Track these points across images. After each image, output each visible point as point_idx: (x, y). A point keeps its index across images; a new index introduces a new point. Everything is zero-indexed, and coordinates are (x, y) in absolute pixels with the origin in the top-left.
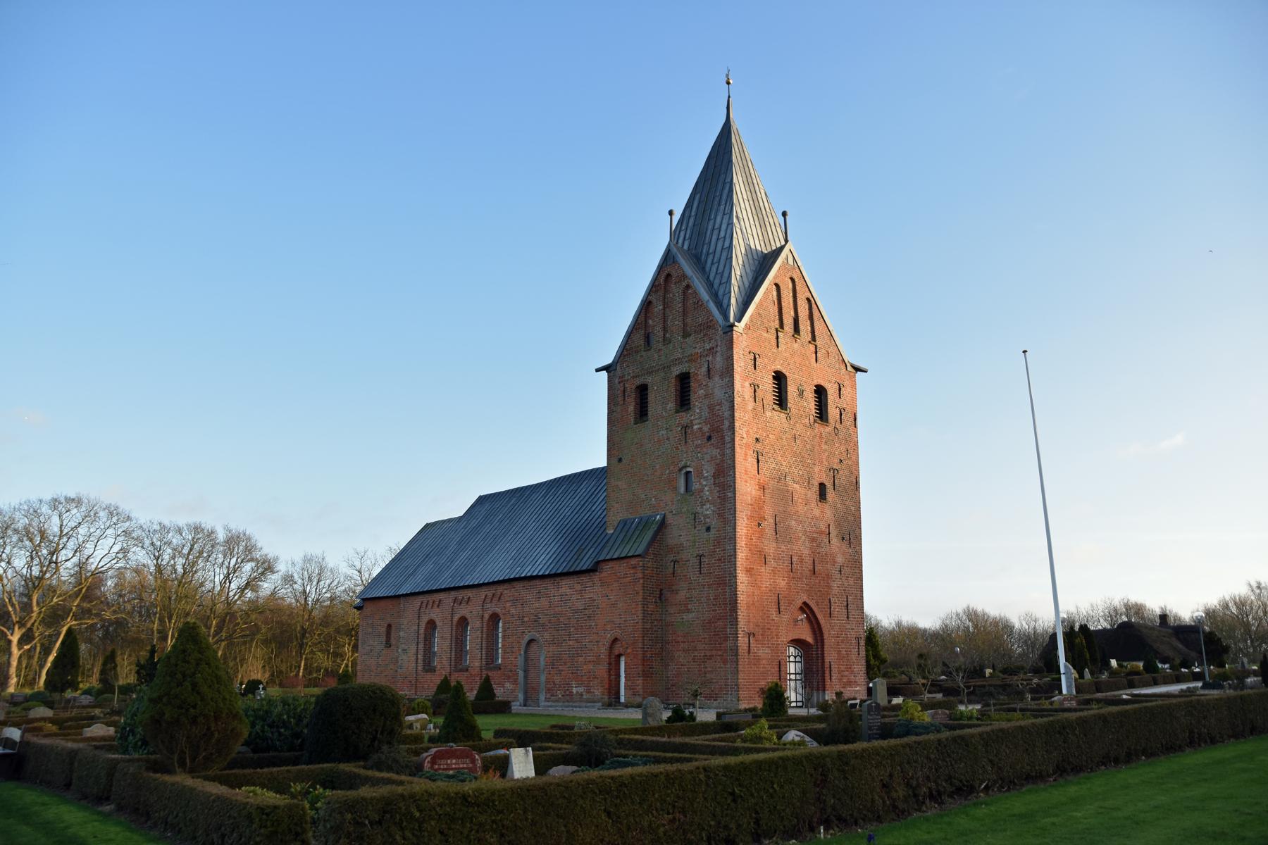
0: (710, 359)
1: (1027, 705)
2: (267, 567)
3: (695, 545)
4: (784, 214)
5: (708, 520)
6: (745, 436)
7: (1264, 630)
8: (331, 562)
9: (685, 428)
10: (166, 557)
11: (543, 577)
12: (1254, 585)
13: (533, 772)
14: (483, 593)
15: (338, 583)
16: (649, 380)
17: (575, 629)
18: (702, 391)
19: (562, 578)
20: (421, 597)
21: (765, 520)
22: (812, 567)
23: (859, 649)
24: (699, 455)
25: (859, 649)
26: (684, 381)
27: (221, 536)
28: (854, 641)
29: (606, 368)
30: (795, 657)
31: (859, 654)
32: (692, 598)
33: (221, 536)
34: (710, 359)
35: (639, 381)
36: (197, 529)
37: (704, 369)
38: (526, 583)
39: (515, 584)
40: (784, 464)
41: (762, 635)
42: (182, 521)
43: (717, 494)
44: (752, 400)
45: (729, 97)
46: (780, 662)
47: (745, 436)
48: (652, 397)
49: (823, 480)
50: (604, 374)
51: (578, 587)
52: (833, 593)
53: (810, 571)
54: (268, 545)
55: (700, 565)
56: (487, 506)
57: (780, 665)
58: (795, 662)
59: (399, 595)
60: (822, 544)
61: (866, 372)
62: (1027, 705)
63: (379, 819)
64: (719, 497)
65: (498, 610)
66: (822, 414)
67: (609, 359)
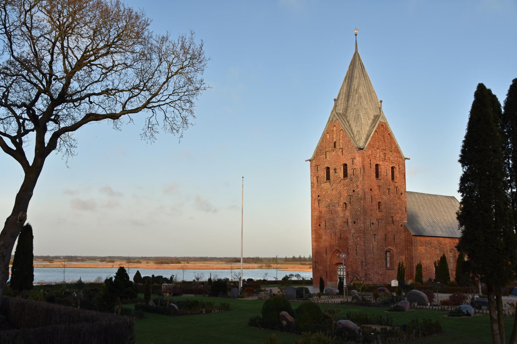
6: (314, 196)
7: (176, 281)
21: (321, 223)
22: (340, 236)
23: (362, 266)
25: (362, 266)
28: (360, 263)
29: (310, 160)
30: (340, 269)
31: (362, 268)
40: (328, 201)
41: (320, 262)
44: (317, 183)
46: (327, 271)
47: (314, 196)
49: (345, 201)
50: (309, 162)
52: (350, 245)
53: (339, 238)
57: (327, 272)
58: (340, 271)
60: (344, 227)
63: (125, 260)
65: (401, 224)
66: (345, 175)
67: (310, 157)
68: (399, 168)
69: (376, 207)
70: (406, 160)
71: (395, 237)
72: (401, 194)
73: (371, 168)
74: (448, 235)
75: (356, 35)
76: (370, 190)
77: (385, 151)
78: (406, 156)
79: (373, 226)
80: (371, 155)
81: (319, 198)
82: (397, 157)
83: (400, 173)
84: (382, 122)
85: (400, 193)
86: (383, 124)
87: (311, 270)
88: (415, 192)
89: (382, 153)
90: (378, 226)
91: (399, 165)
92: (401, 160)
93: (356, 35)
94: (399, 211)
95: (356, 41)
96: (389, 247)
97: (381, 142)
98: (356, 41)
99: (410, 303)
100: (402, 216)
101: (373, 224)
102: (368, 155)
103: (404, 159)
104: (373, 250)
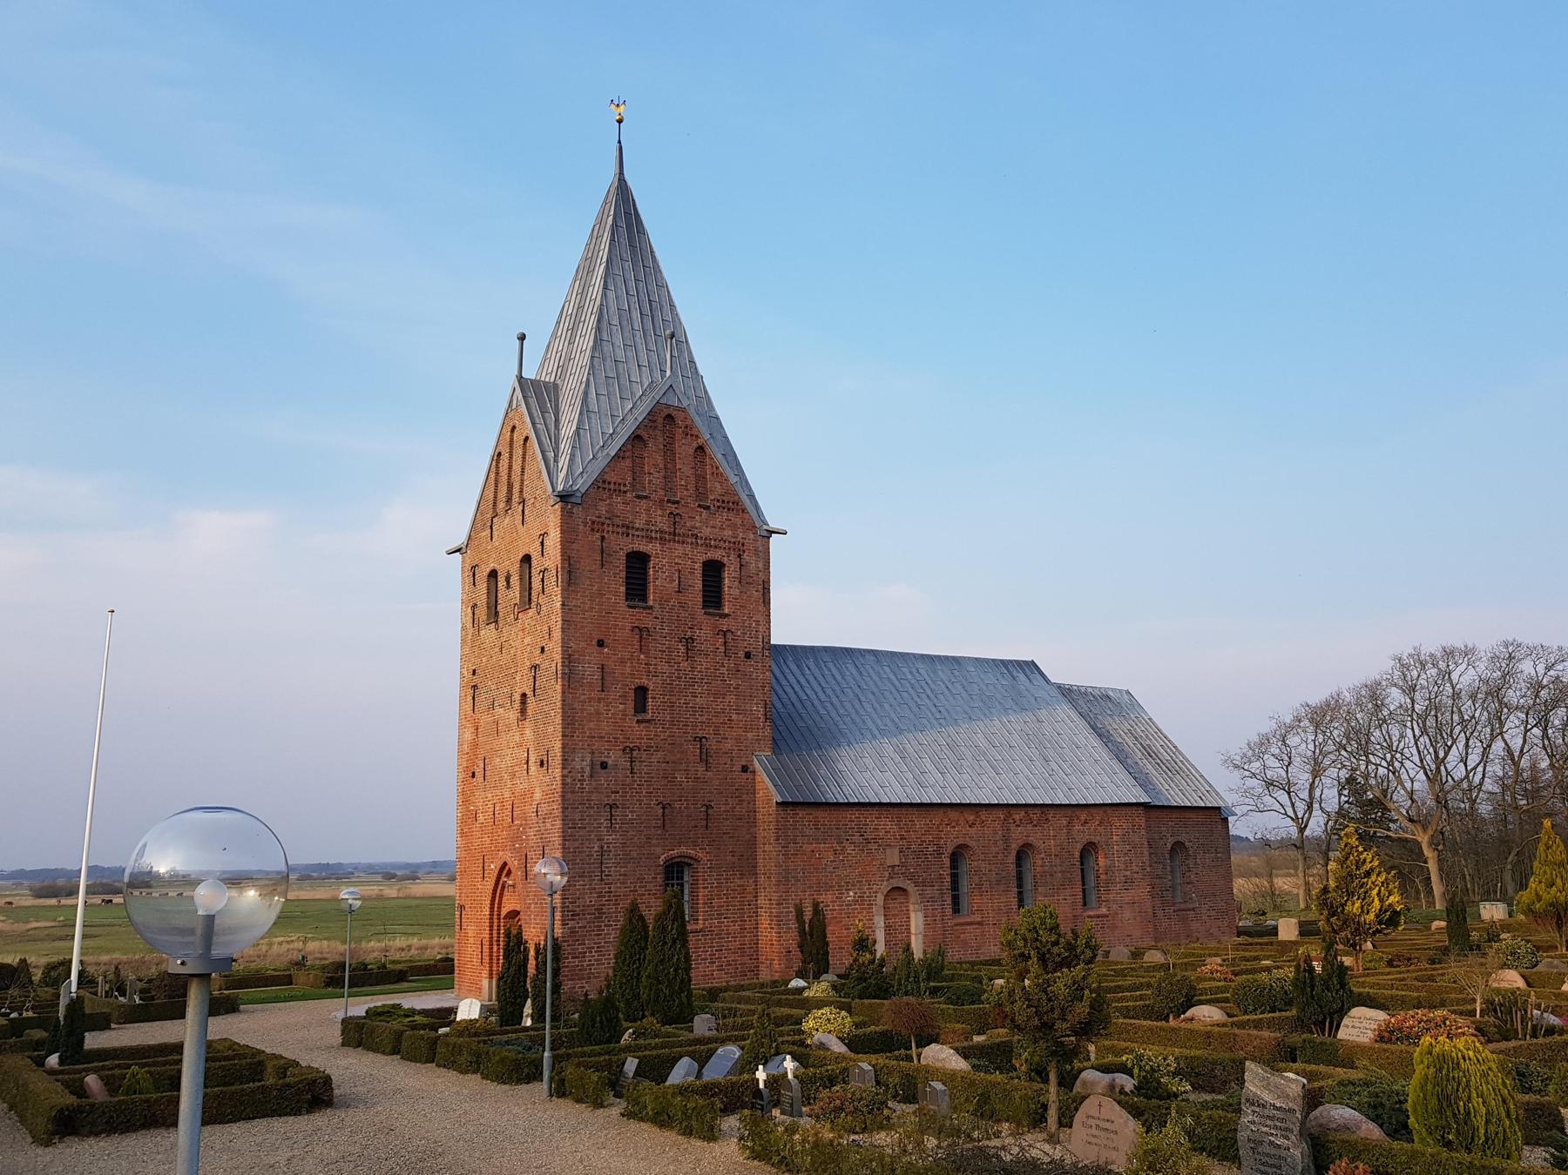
68: (741, 565)
69: (620, 703)
70: (773, 535)
71: (710, 811)
72: (748, 655)
73: (602, 565)
74: (1135, 797)
75: (620, 121)
76: (594, 642)
77: (676, 506)
78: (773, 525)
79: (603, 778)
80: (607, 521)
81: (476, 680)
82: (734, 527)
83: (744, 582)
84: (668, 406)
85: (741, 654)
86: (674, 413)
87: (216, 928)
88: (864, 650)
89: (659, 512)
90: (631, 773)
91: (739, 556)
92: (752, 536)
93: (620, 121)
94: (734, 717)
95: (619, 142)
96: (683, 850)
97: (657, 475)
98: (619, 142)
99: (699, 1066)
100: (750, 735)
101: (604, 766)
102: (593, 522)
103: (765, 534)
104: (602, 863)
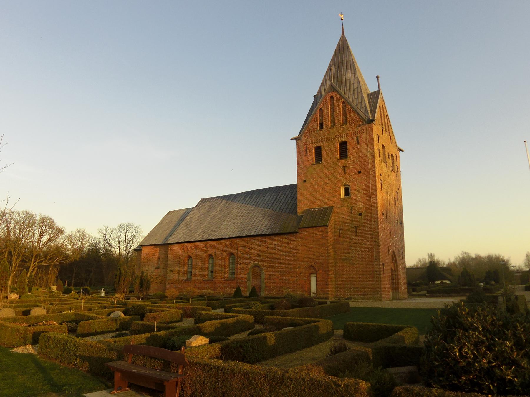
0: (359, 135)
1: (129, 284)
2: (60, 231)
3: (353, 222)
4: (377, 77)
5: (360, 210)
8: (87, 232)
9: (344, 168)
10: (12, 226)
11: (261, 236)
12: (430, 254)
13: (191, 319)
14: (223, 243)
15: (92, 240)
16: (322, 145)
17: (284, 261)
18: (355, 150)
19: (276, 236)
20: (182, 244)
24: (353, 180)
26: (344, 146)
27: (38, 218)
32: (351, 247)
33: (38, 218)
34: (359, 135)
35: (318, 145)
36: (27, 213)
37: (355, 140)
38: (251, 239)
39: (244, 239)
42: (21, 211)
43: (366, 198)
45: (343, 25)
48: (323, 153)
51: (286, 240)
54: (59, 223)
55: (356, 231)
56: (208, 203)
59: (168, 244)
61: (403, 151)
62: (129, 284)
64: (366, 199)
67: (296, 135)
